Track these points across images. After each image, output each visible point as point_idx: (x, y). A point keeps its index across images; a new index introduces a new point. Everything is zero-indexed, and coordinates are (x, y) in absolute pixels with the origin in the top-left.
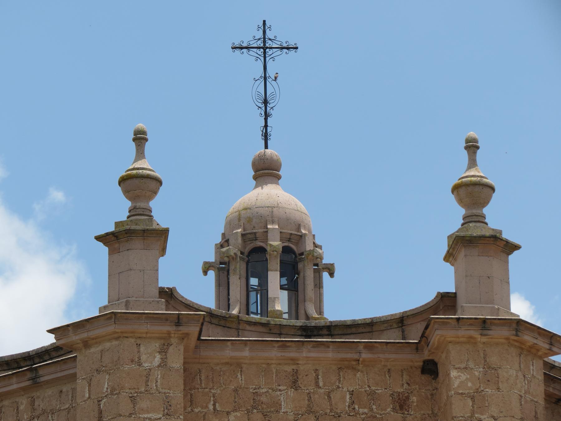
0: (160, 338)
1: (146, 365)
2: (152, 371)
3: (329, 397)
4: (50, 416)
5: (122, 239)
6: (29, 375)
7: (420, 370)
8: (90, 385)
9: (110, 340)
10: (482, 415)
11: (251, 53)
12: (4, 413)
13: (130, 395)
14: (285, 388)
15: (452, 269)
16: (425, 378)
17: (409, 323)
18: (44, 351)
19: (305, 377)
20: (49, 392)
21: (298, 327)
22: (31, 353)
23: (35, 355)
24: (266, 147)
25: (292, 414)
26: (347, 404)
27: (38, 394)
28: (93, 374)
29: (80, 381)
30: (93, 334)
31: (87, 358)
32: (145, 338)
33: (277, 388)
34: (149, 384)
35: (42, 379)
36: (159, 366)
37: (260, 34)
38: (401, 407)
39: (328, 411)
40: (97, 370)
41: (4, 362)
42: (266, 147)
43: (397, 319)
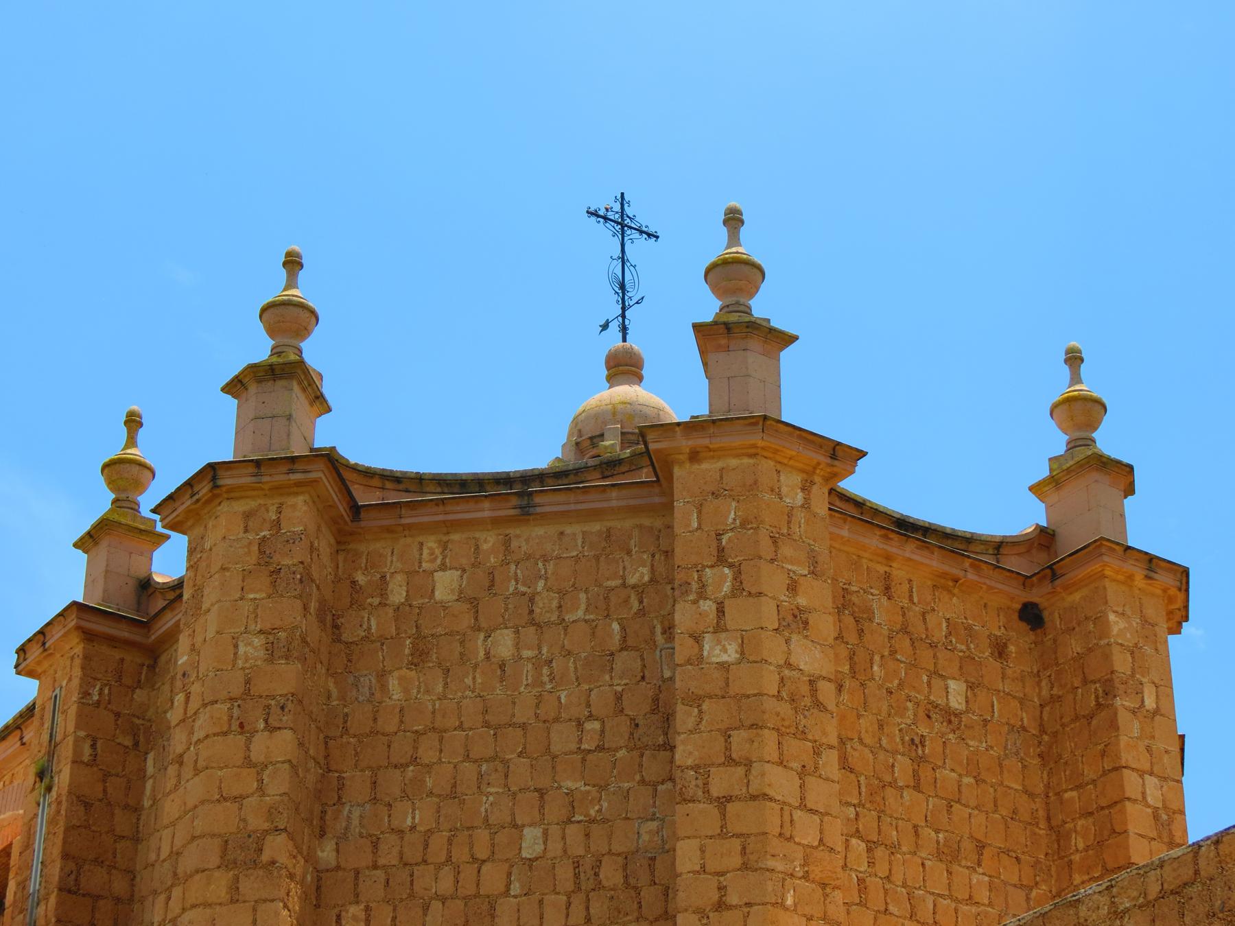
0: (802, 471)
1: (788, 501)
2: (795, 510)
3: (924, 620)
4: (540, 564)
5: (736, 335)
6: (515, 501)
7: (1017, 614)
8: (699, 513)
9: (738, 456)
10: (1143, 677)
11: (607, 225)
12: (450, 550)
13: (771, 534)
14: (877, 592)
15: (1043, 505)
16: (1023, 626)
17: (1005, 553)
18: (535, 475)
19: (898, 585)
20: (539, 531)
21: (895, 519)
22: (512, 474)
23: (519, 477)
24: (624, 340)
25: (886, 628)
26: (944, 633)
27: (518, 532)
28: (706, 498)
29: (682, 504)
30: (716, 443)
31: (693, 476)
32: (785, 465)
33: (869, 590)
34: (792, 526)
35: (539, 510)
36: (802, 506)
37: (617, 207)
38: (1000, 654)
39: (924, 636)
40: (713, 494)
41: (459, 482)
42: (624, 340)
43: (995, 542)
